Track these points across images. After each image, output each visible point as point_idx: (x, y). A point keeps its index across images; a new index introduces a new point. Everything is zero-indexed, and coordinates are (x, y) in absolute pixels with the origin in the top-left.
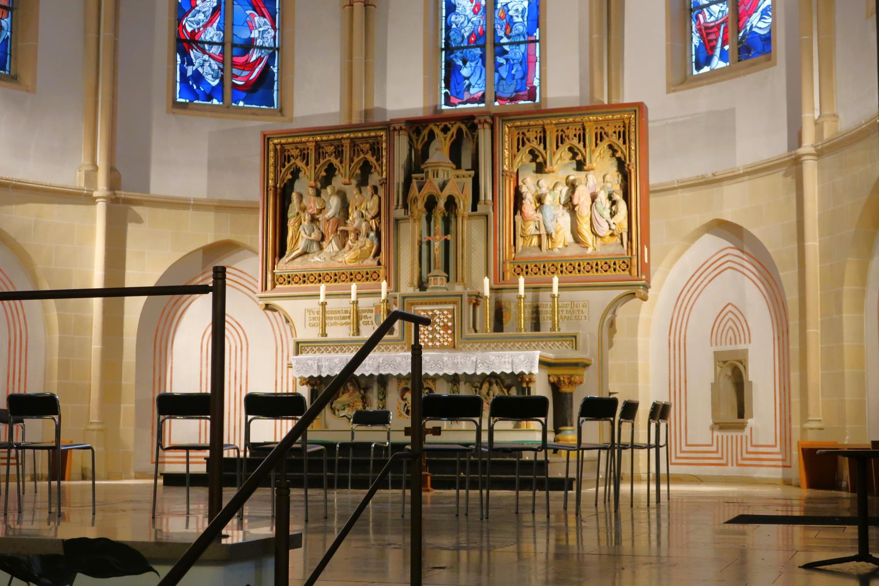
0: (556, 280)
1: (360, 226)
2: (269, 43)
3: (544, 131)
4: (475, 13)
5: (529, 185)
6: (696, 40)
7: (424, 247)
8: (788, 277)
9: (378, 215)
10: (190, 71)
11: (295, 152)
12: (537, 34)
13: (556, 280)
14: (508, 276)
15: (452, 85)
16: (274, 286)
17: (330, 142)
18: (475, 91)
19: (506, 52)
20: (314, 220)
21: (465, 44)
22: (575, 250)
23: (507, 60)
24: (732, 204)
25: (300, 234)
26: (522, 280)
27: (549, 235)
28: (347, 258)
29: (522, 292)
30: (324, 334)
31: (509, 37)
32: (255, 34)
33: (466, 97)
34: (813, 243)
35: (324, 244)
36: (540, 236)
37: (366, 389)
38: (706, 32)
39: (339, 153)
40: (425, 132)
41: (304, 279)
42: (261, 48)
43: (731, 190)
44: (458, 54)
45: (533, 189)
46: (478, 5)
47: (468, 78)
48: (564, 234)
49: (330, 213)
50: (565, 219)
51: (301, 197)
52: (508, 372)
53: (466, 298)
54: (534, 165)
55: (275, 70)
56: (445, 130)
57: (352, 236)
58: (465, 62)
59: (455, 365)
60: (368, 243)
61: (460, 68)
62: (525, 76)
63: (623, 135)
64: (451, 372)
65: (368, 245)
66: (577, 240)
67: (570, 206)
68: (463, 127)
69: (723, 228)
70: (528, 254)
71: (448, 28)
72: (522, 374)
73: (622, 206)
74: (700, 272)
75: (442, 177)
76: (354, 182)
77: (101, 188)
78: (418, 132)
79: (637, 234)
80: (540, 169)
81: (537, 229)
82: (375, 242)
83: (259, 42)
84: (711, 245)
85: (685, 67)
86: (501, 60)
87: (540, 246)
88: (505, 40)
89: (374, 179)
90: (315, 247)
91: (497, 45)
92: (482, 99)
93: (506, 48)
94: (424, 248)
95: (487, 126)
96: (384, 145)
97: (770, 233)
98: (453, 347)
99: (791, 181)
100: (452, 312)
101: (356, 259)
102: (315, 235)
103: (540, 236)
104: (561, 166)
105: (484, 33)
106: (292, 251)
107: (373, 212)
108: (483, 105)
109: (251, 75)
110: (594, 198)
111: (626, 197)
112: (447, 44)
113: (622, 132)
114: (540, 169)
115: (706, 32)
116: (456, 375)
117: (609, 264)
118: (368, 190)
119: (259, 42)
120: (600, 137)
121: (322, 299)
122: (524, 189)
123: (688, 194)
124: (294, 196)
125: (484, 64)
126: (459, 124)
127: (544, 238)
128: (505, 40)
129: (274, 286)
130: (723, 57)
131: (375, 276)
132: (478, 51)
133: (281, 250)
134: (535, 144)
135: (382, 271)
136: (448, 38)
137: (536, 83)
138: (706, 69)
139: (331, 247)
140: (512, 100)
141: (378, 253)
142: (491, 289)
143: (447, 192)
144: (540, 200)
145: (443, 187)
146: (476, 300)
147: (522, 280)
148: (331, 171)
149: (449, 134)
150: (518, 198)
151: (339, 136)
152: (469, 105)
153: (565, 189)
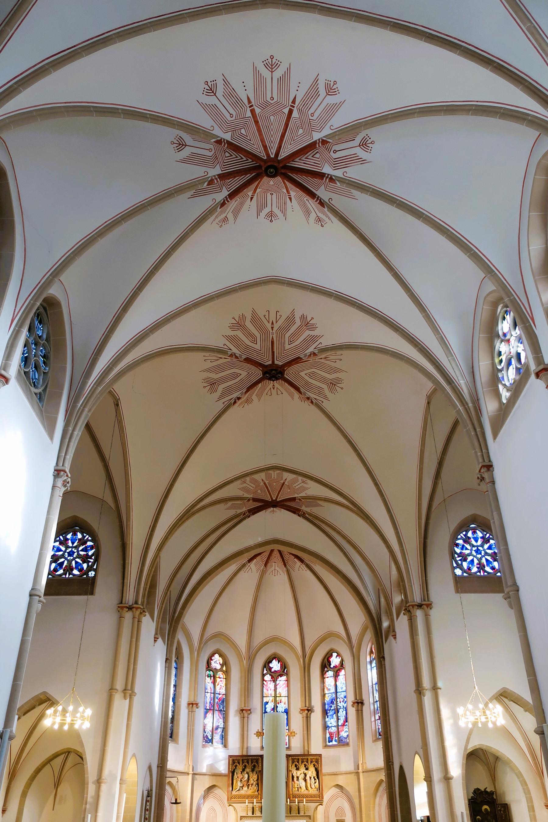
6: (328, 735)
8: (356, 801)
10: (205, 734)
11: (236, 761)
17: (246, 759)
20: (241, 781)
22: (306, 792)
24: (341, 780)
27: (300, 788)
29: (297, 803)
34: (362, 794)
38: (331, 734)
39: (248, 763)
43: (340, 777)
48: (304, 787)
50: (304, 783)
63: (317, 762)
66: (307, 789)
67: (305, 780)
69: (338, 786)
73: (317, 780)
74: (333, 796)
77: (191, 772)
79: (320, 789)
80: (298, 769)
84: (335, 790)
85: (326, 742)
89: (256, 769)
97: (351, 789)
99: (356, 777)
102: (242, 785)
104: (303, 769)
110: (310, 778)
111: (318, 778)
113: (317, 760)
114: (298, 769)
115: (331, 734)
117: (315, 796)
120: (311, 762)
121: (247, 804)
123: (330, 777)
130: (335, 741)
138: (331, 743)
139: (245, 788)
141: (258, 790)
144: (298, 778)
148: (245, 766)
150: (293, 777)
153: (303, 775)
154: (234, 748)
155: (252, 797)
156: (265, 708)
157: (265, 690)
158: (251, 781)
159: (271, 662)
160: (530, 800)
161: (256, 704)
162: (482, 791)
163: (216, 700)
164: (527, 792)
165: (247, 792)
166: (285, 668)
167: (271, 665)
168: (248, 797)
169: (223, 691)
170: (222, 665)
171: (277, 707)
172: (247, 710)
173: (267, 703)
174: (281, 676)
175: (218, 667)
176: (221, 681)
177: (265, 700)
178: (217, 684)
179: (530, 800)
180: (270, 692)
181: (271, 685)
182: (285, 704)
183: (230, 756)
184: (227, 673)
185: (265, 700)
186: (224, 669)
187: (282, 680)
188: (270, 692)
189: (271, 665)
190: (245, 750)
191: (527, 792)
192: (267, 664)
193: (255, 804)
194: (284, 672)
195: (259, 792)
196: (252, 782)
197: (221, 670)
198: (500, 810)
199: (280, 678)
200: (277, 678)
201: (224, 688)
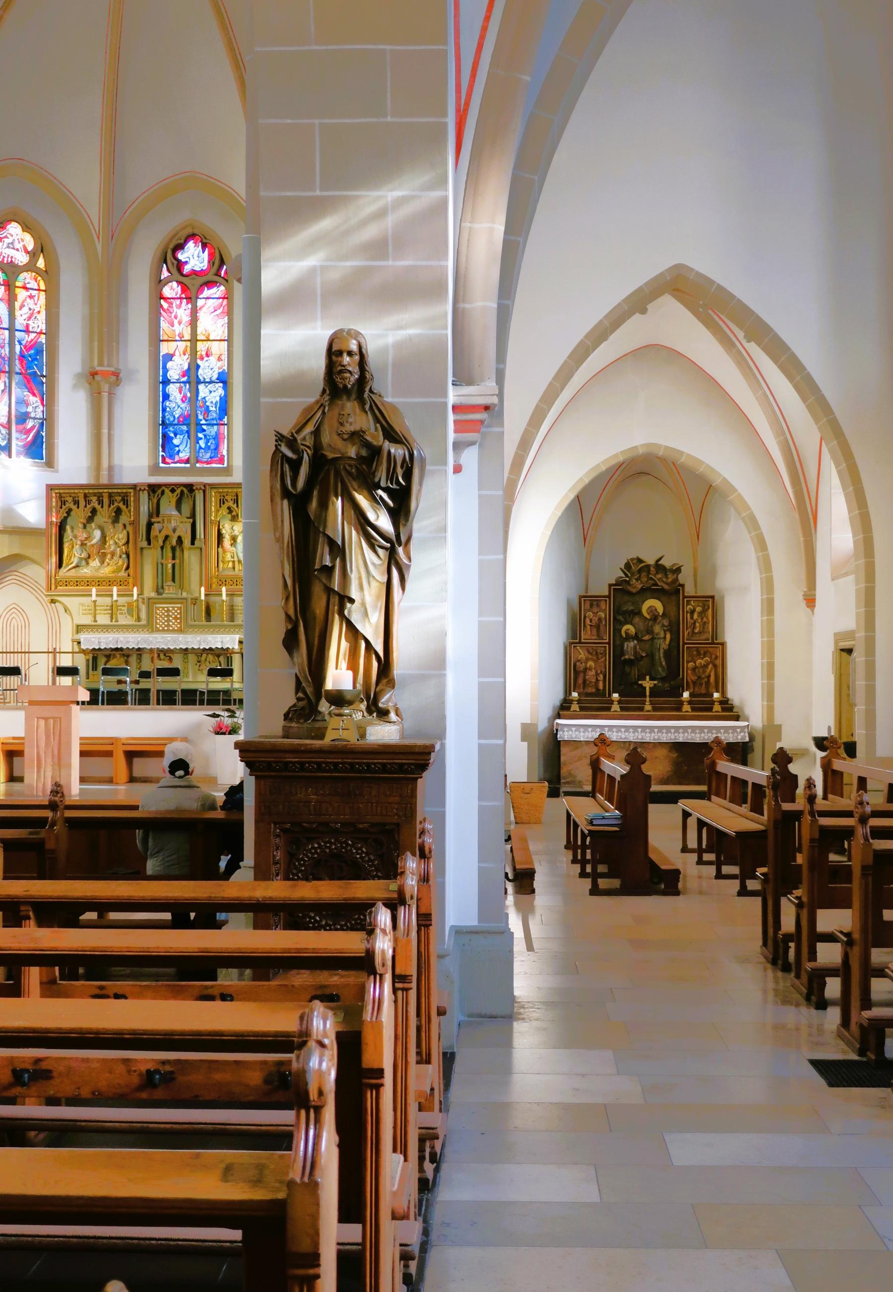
0: (94, 590)
1: (115, 550)
2: (40, 415)
3: (237, 496)
4: (183, 401)
5: (226, 530)
7: (160, 566)
9: (128, 542)
11: (70, 499)
12: (225, 420)
13: (94, 590)
14: (214, 586)
15: (167, 449)
16: (56, 587)
17: (95, 494)
18: (184, 455)
19: (204, 430)
20: (83, 544)
21: (176, 422)
23: (205, 436)
25: (73, 554)
26: (224, 589)
28: (106, 571)
29: (224, 597)
30: (95, 621)
31: (206, 420)
32: (30, 409)
33: (177, 458)
35: (90, 561)
36: (234, 562)
37: (128, 656)
39: (101, 502)
40: (159, 491)
41: (77, 583)
42: (34, 418)
44: (171, 429)
45: (229, 531)
46: (185, 396)
47: (178, 446)
49: (94, 541)
51: (72, 528)
52: (220, 647)
53: (189, 600)
54: (230, 516)
55: (44, 434)
56: (173, 491)
57: (109, 556)
58: (176, 435)
59: (187, 642)
60: (122, 562)
61: (172, 438)
62: (217, 448)
64: (184, 647)
65: (120, 563)
68: (185, 490)
70: (226, 573)
71: (164, 410)
72: (228, 648)
75: (173, 524)
76: (110, 521)
78: (154, 492)
81: (233, 557)
82: (126, 560)
83: (33, 415)
86: (200, 435)
87: (234, 568)
88: (203, 422)
89: (124, 519)
90: (84, 563)
91: (198, 424)
92: (187, 461)
93: (204, 427)
94: (160, 569)
95: (201, 491)
96: (132, 499)
98: (180, 631)
100: (180, 608)
101: (113, 572)
102: (84, 555)
103: (234, 562)
105: (188, 416)
106: (68, 565)
107: (124, 541)
108: (188, 465)
109: (27, 438)
112: (163, 421)
114: (234, 518)
116: (187, 649)
118: (120, 525)
119: (33, 415)
121: (94, 598)
122: (223, 531)
124: (68, 528)
125: (189, 437)
126: (182, 488)
127: (236, 563)
128: (203, 422)
129: (56, 587)
131: (126, 583)
132: (185, 428)
133: (60, 565)
134: (231, 504)
135: (131, 580)
136: (164, 417)
137: (225, 453)
139: (95, 563)
140: (208, 463)
141: (128, 568)
142: (227, 595)
143: (177, 534)
145: (174, 531)
146: (195, 601)
147: (224, 589)
148: (94, 511)
149: (176, 493)
150: (220, 536)
151: (101, 491)
152: (178, 465)
154: (73, 465)
155: (110, 582)
156: (166, 371)
157: (164, 325)
158: (111, 545)
159: (180, 247)
160: (768, 586)
161: (135, 356)
162: (648, 566)
163: (18, 348)
164: (766, 565)
165: (97, 570)
166: (222, 262)
167: (181, 256)
168: (99, 582)
169: (39, 323)
170: (33, 255)
171: (198, 367)
172: (105, 374)
173: (170, 357)
174: (210, 284)
175: (22, 259)
176: (31, 297)
177: (165, 348)
178: (17, 305)
179: (768, 586)
180: (177, 329)
181: (183, 312)
182: (219, 359)
183: (50, 488)
184: (50, 275)
185: (165, 348)
186: (41, 263)
187: (211, 300)
188: (177, 329)
189: (181, 256)
190: (104, 473)
191: (766, 565)
192: (170, 255)
193: (115, 598)
194: (218, 274)
195: (131, 570)
196: (112, 548)
197: (30, 267)
198: (692, 612)
199: (207, 293)
200: (200, 289)
201: (42, 317)
